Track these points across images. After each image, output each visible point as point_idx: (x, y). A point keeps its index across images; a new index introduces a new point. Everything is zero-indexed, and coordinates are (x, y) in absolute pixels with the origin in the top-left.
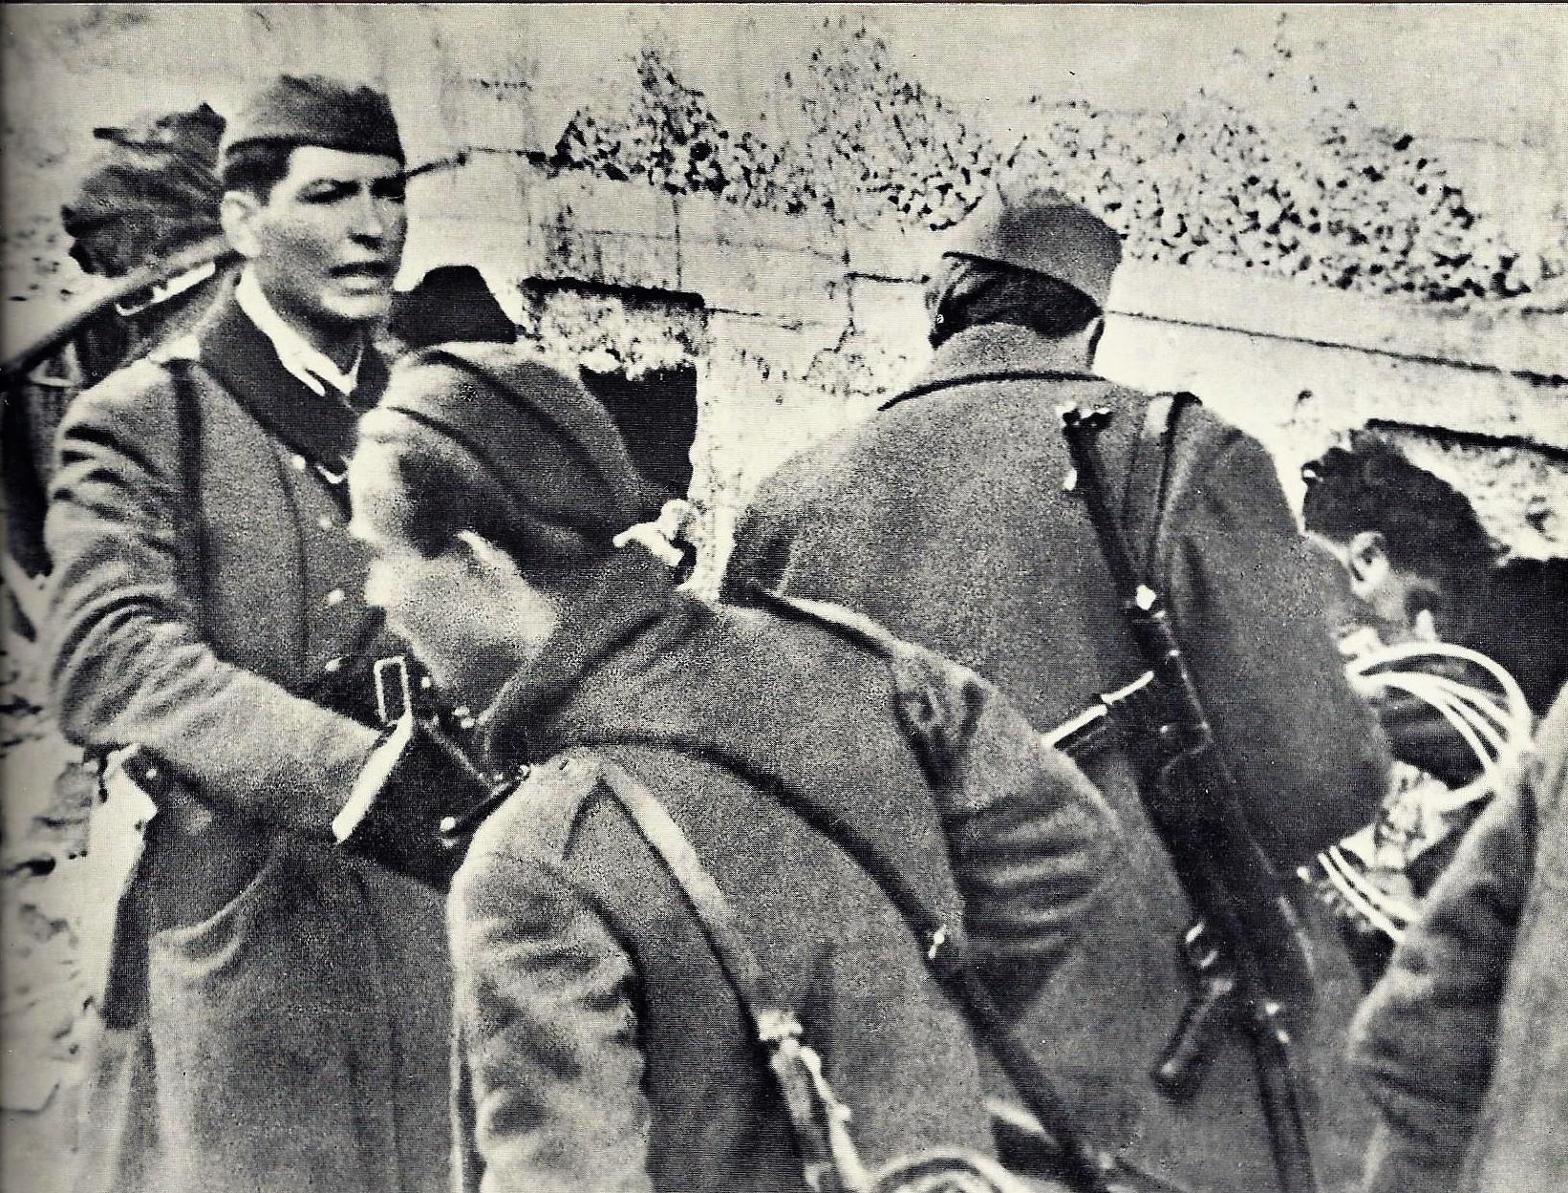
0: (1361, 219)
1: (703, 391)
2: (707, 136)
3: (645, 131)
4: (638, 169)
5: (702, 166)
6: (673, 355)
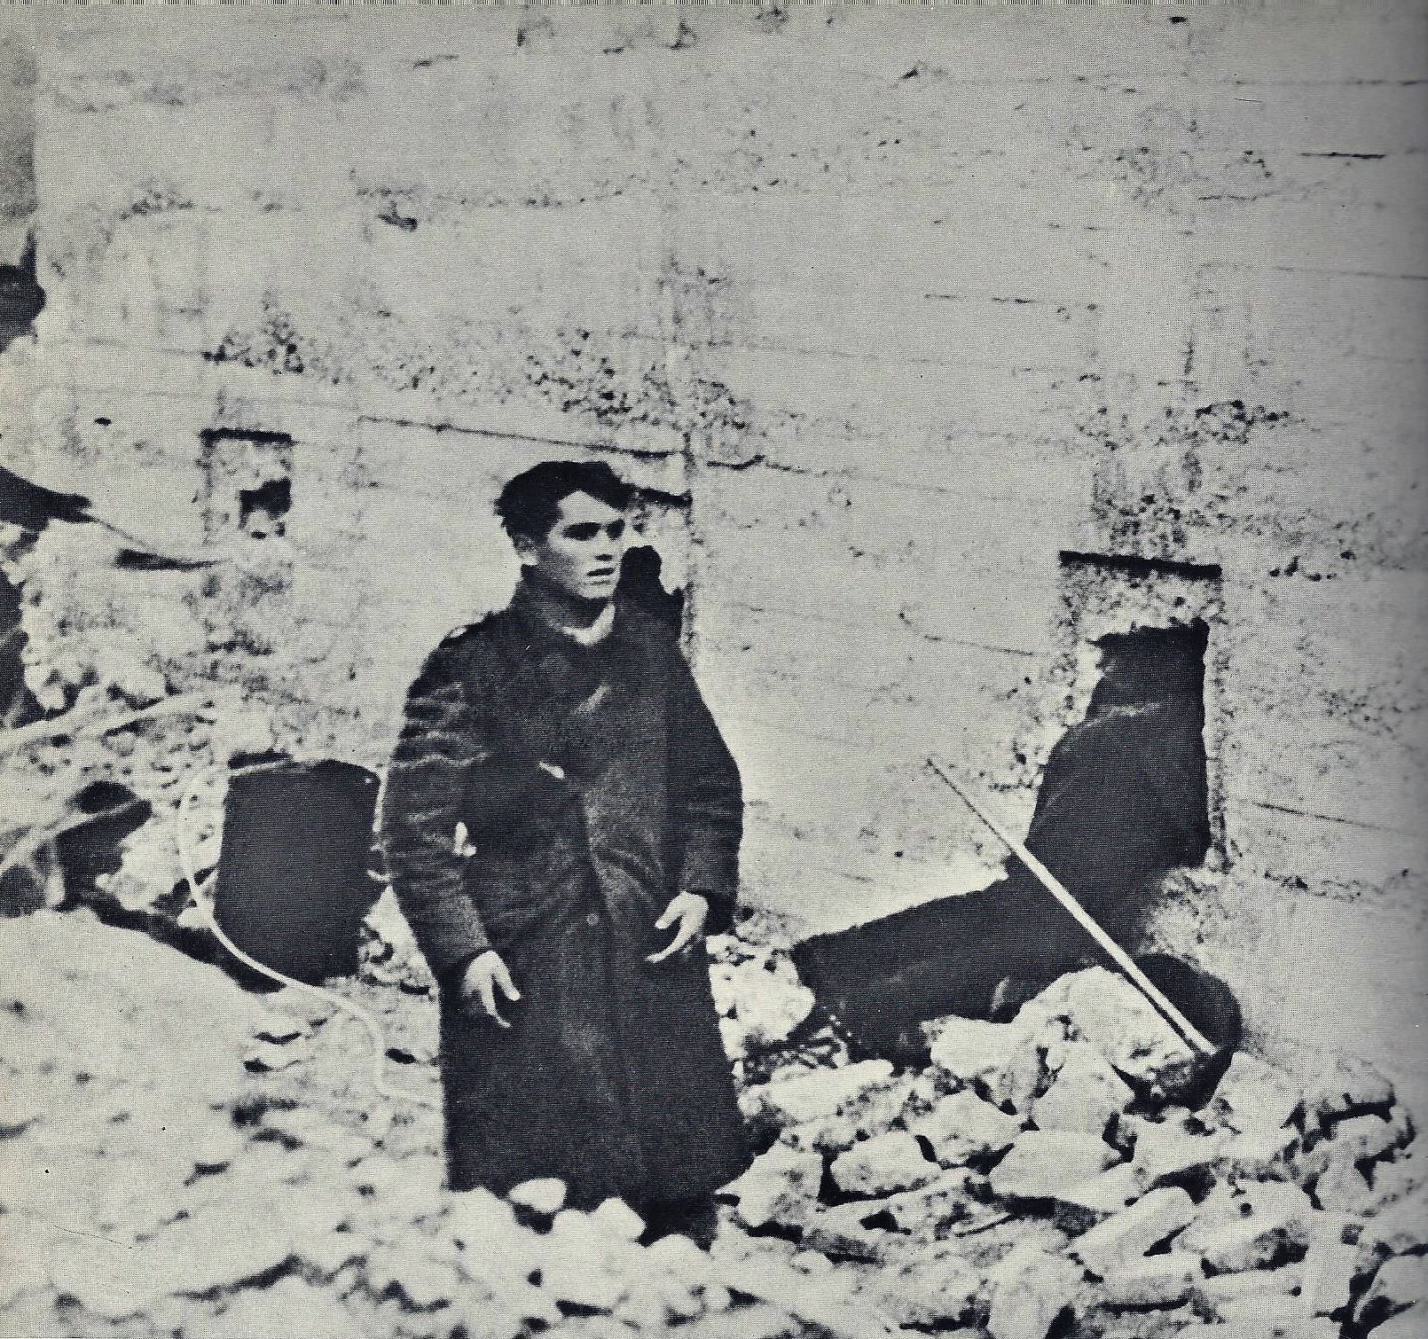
0: (572, 376)
1: (293, 491)
2: (293, 341)
3: (263, 338)
4: (260, 360)
5: (292, 356)
6: (278, 473)
